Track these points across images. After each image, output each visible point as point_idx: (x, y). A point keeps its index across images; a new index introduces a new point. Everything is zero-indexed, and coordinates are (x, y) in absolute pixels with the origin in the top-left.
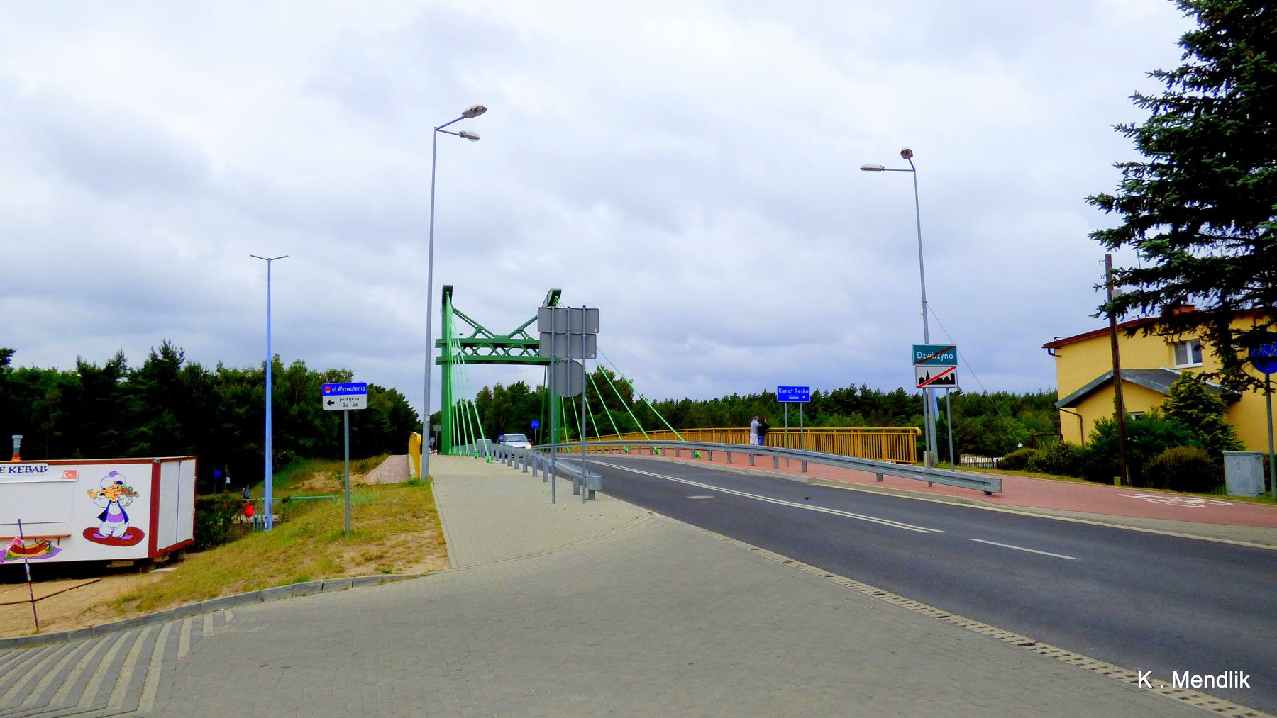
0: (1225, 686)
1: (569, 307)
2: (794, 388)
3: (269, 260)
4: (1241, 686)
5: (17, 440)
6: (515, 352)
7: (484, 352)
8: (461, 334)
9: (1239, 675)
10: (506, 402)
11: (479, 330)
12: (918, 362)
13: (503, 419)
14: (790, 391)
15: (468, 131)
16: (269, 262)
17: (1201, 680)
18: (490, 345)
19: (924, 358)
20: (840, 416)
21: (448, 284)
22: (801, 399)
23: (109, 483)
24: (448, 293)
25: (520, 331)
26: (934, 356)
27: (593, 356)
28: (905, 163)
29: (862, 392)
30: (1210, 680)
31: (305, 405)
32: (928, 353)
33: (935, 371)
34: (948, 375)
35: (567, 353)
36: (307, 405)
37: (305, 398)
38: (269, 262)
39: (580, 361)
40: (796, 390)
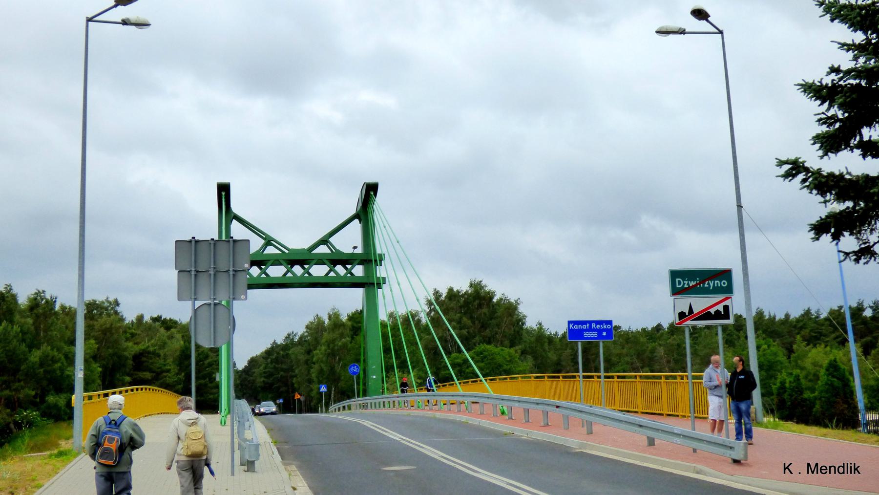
2: (590, 322)
6: (319, 271)
7: (276, 272)
10: (342, 336)
12: (676, 292)
13: (340, 360)
14: (584, 327)
15: (133, 17)
18: (282, 262)
19: (686, 286)
20: (828, 348)
22: (600, 336)
24: (223, 194)
25: (324, 241)
26: (699, 284)
27: (243, 297)
28: (703, 25)
29: (874, 310)
30: (717, 283)
31: (49, 348)
32: (690, 280)
33: (700, 303)
34: (720, 308)
35: (211, 294)
36: (52, 349)
37: (50, 341)
40: (593, 325)
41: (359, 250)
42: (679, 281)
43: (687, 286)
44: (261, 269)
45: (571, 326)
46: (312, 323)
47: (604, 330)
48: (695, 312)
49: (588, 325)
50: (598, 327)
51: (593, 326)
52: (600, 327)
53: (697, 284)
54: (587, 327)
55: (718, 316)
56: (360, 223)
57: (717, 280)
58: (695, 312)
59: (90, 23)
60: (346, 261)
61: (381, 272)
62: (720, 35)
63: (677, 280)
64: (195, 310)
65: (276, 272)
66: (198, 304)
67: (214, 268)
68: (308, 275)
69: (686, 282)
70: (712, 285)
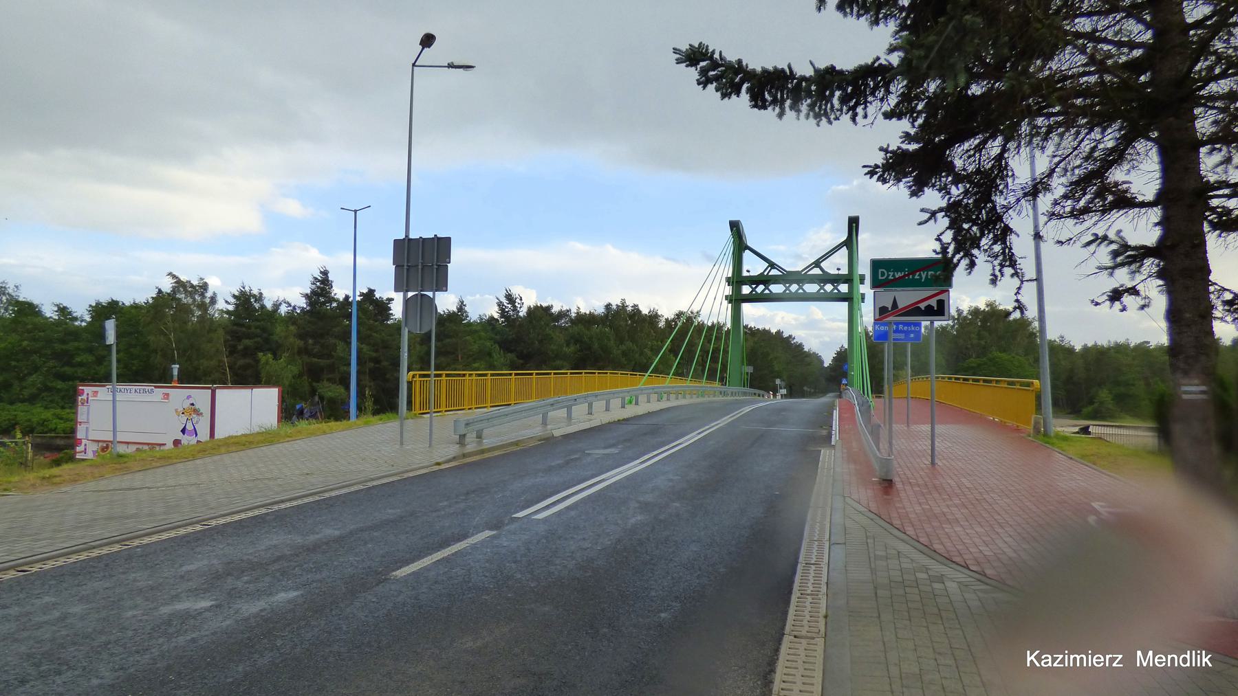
0: (1188, 665)
1: (421, 237)
3: (355, 211)
4: (1204, 665)
5: (176, 368)
8: (839, 269)
9: (1201, 654)
11: (772, 265)
16: (356, 213)
17: (1102, 660)
19: (891, 278)
21: (853, 214)
23: (187, 404)
25: (817, 264)
26: (908, 275)
27: (444, 288)
30: (1173, 659)
34: (933, 302)
38: (356, 213)
39: (430, 294)
45: (877, 327)
47: (912, 332)
53: (905, 275)
55: (929, 312)
58: (900, 307)
59: (415, 68)
60: (836, 280)
61: (728, 290)
63: (880, 270)
64: (406, 301)
65: (811, 288)
66: (410, 294)
67: (422, 263)
69: (891, 274)
70: (924, 276)
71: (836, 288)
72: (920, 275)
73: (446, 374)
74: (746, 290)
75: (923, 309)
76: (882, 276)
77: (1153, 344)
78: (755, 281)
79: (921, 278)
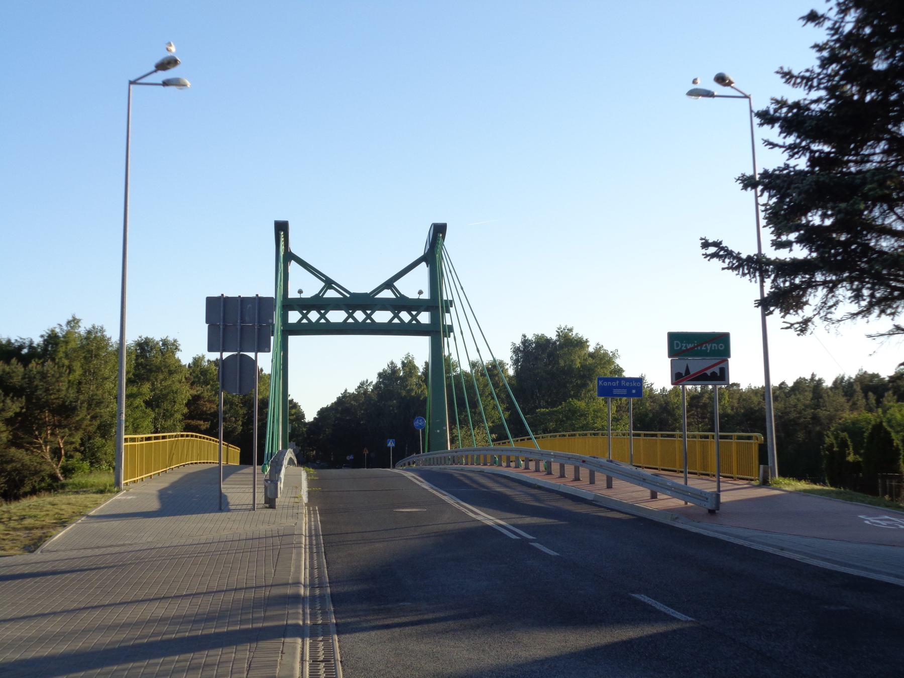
6: (382, 317)
11: (329, 283)
14: (614, 384)
19: (684, 348)
25: (389, 284)
26: (697, 346)
27: (266, 349)
28: (727, 91)
30: (715, 347)
39: (252, 355)
41: (426, 296)
42: (677, 343)
43: (685, 349)
44: (320, 313)
45: (600, 383)
46: (385, 371)
48: (692, 372)
49: (618, 382)
50: (627, 384)
51: (622, 383)
52: (630, 385)
53: (695, 347)
54: (616, 384)
56: (428, 267)
57: (714, 343)
59: (132, 86)
62: (747, 100)
63: (675, 342)
65: (336, 316)
68: (370, 322)
70: (709, 348)
71: (350, 316)
72: (706, 347)
73: (155, 437)
74: (424, 318)
75: (709, 375)
76: (677, 347)
77: (178, 355)
78: (304, 305)
79: (707, 349)
